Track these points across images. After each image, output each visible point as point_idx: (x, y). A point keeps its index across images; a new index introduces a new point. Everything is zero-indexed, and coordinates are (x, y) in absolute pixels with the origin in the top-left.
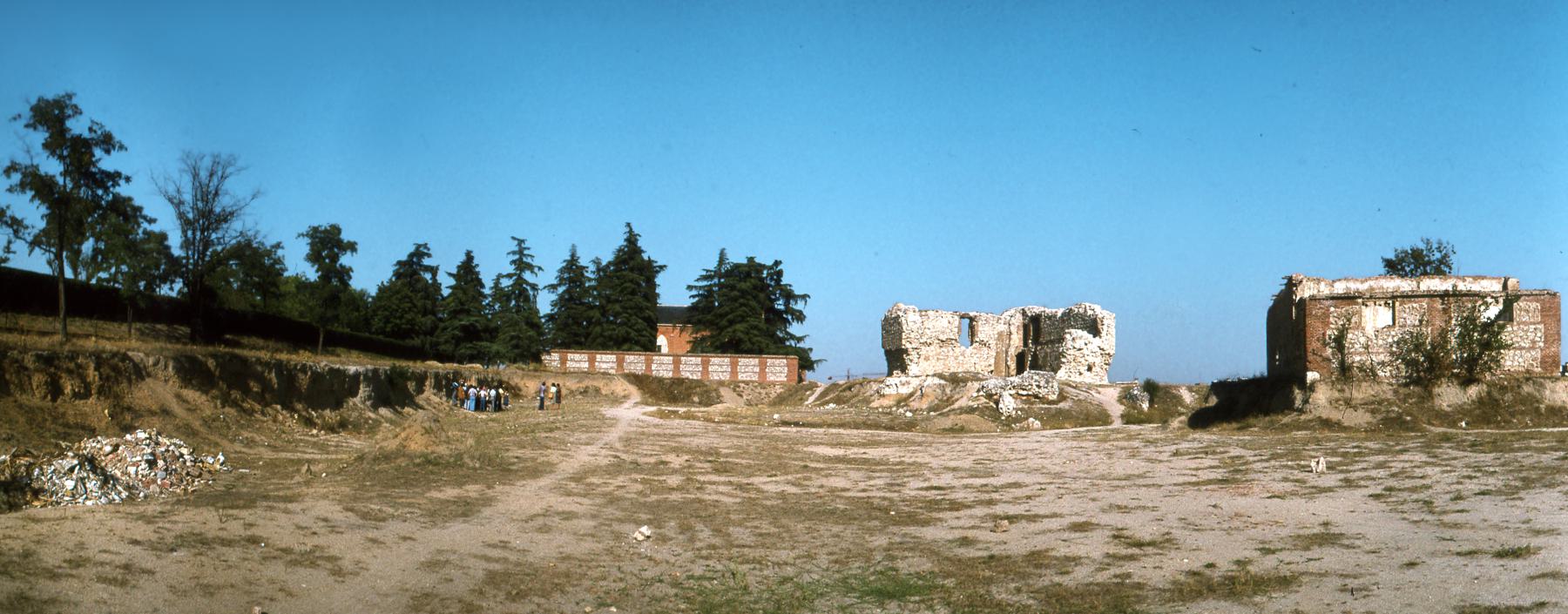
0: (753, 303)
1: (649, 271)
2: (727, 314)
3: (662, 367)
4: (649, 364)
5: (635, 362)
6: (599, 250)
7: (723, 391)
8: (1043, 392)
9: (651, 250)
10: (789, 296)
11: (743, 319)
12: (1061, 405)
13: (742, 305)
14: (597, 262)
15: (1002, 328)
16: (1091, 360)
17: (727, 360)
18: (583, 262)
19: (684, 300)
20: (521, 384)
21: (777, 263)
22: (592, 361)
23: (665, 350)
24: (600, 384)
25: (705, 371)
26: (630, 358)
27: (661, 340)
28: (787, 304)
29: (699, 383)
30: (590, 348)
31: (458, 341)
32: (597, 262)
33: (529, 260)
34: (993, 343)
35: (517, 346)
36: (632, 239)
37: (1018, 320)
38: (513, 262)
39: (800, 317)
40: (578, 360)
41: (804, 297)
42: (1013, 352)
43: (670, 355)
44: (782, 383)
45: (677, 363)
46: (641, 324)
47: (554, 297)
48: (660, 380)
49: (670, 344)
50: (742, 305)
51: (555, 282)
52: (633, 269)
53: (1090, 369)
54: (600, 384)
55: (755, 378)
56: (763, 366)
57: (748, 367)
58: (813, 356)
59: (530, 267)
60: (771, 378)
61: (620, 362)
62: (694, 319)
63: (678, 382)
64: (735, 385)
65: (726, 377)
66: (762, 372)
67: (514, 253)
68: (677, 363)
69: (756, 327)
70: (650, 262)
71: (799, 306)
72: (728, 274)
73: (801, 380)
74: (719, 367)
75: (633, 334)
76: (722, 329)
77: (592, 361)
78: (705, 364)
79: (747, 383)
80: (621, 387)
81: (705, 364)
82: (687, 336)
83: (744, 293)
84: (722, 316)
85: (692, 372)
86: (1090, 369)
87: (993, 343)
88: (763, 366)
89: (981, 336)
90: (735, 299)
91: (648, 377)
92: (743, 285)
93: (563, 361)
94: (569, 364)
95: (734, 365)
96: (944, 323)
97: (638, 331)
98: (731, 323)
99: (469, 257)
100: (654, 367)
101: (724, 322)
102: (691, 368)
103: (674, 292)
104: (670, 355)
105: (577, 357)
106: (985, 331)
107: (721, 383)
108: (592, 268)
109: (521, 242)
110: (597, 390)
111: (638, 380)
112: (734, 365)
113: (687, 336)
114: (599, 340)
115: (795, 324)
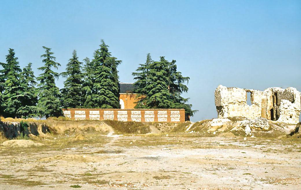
0: (164, 83)
1: (113, 64)
2: (152, 88)
3: (122, 117)
4: (116, 114)
5: (109, 114)
6: (87, 54)
7: (151, 128)
8: (263, 126)
9: (114, 53)
10: (180, 79)
11: (159, 90)
12: (270, 132)
13: (158, 83)
14: (87, 60)
15: (264, 97)
16: (291, 113)
17: (153, 112)
18: (80, 60)
19: (132, 81)
20: (56, 128)
21: (174, 62)
22: (87, 114)
23: (123, 107)
24: (94, 126)
25: (143, 117)
26: (106, 112)
27: (122, 102)
28: (180, 82)
29: (140, 124)
30: (86, 107)
31: (17, 106)
32: (87, 60)
33: (53, 60)
34: (260, 104)
35: (50, 108)
36: (104, 49)
37: (270, 94)
38: (45, 60)
39: (186, 89)
40: (80, 114)
41: (188, 78)
42: (269, 108)
43: (127, 110)
44: (178, 123)
45: (129, 114)
46: (111, 94)
47: (65, 79)
48: (122, 123)
49: (126, 105)
50: (158, 83)
51: (66, 71)
52: (105, 62)
53: (291, 117)
54: (94, 126)
55: (166, 120)
56: (169, 114)
57: (162, 114)
58: (192, 109)
59: (54, 63)
60: (173, 120)
61: (102, 115)
62: (137, 91)
63: (131, 123)
64: (156, 125)
65: (152, 120)
66: (169, 118)
67: (45, 56)
68: (129, 114)
69: (165, 95)
70: (114, 59)
71: (185, 83)
72: (152, 67)
73: (256, 104)
74: (149, 115)
75: (107, 99)
76: (150, 96)
77: (87, 114)
78: (143, 114)
79: (162, 123)
80: (104, 127)
81: (143, 114)
82: (133, 100)
83: (159, 77)
84: (149, 89)
85: (137, 118)
86: (291, 117)
87: (260, 104)
88: (169, 114)
89: (255, 101)
90: (156, 80)
91: (116, 122)
92: (159, 73)
93: (73, 115)
94: (76, 116)
95: (156, 114)
96: (240, 94)
97: (109, 97)
98: (154, 92)
99: (11, 51)
100: (118, 116)
101: (151, 93)
102: (136, 116)
103: (126, 76)
104: (127, 110)
105: (79, 112)
106: (258, 97)
107: (150, 124)
108: (85, 63)
109: (48, 50)
110: (94, 129)
111: (113, 124)
112: (156, 114)
113: (133, 100)
114: (90, 103)
115: (183, 92)
